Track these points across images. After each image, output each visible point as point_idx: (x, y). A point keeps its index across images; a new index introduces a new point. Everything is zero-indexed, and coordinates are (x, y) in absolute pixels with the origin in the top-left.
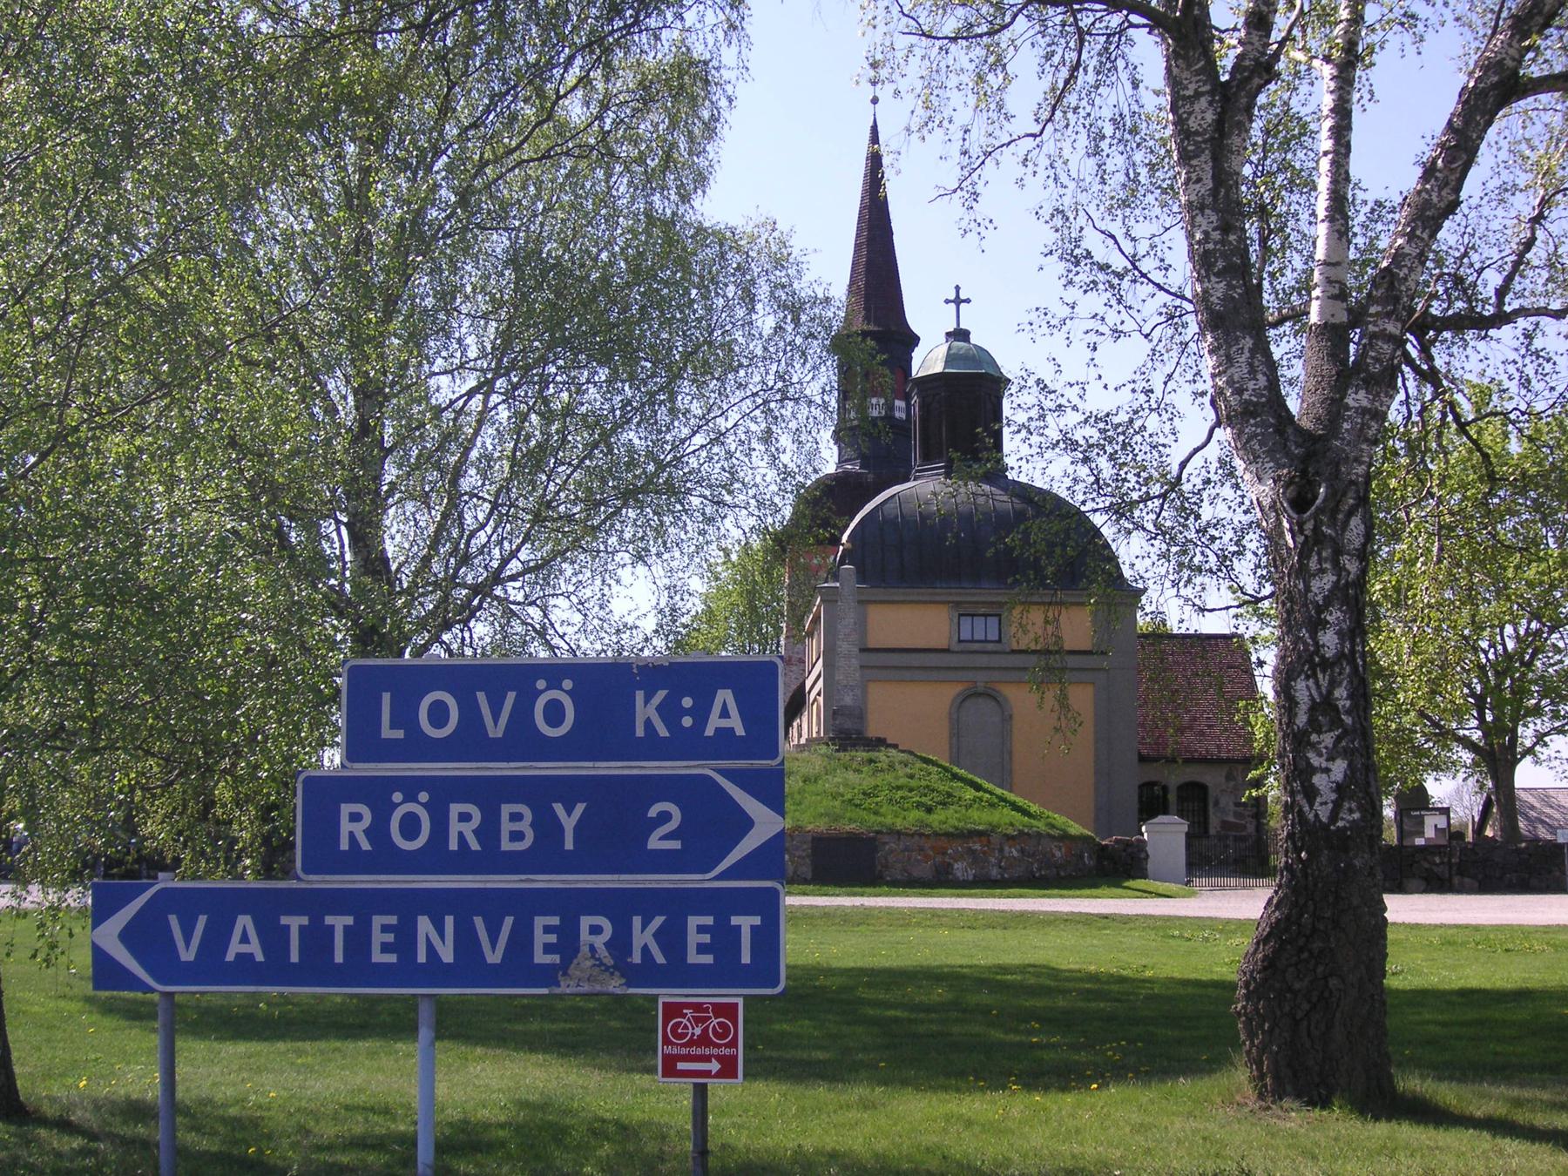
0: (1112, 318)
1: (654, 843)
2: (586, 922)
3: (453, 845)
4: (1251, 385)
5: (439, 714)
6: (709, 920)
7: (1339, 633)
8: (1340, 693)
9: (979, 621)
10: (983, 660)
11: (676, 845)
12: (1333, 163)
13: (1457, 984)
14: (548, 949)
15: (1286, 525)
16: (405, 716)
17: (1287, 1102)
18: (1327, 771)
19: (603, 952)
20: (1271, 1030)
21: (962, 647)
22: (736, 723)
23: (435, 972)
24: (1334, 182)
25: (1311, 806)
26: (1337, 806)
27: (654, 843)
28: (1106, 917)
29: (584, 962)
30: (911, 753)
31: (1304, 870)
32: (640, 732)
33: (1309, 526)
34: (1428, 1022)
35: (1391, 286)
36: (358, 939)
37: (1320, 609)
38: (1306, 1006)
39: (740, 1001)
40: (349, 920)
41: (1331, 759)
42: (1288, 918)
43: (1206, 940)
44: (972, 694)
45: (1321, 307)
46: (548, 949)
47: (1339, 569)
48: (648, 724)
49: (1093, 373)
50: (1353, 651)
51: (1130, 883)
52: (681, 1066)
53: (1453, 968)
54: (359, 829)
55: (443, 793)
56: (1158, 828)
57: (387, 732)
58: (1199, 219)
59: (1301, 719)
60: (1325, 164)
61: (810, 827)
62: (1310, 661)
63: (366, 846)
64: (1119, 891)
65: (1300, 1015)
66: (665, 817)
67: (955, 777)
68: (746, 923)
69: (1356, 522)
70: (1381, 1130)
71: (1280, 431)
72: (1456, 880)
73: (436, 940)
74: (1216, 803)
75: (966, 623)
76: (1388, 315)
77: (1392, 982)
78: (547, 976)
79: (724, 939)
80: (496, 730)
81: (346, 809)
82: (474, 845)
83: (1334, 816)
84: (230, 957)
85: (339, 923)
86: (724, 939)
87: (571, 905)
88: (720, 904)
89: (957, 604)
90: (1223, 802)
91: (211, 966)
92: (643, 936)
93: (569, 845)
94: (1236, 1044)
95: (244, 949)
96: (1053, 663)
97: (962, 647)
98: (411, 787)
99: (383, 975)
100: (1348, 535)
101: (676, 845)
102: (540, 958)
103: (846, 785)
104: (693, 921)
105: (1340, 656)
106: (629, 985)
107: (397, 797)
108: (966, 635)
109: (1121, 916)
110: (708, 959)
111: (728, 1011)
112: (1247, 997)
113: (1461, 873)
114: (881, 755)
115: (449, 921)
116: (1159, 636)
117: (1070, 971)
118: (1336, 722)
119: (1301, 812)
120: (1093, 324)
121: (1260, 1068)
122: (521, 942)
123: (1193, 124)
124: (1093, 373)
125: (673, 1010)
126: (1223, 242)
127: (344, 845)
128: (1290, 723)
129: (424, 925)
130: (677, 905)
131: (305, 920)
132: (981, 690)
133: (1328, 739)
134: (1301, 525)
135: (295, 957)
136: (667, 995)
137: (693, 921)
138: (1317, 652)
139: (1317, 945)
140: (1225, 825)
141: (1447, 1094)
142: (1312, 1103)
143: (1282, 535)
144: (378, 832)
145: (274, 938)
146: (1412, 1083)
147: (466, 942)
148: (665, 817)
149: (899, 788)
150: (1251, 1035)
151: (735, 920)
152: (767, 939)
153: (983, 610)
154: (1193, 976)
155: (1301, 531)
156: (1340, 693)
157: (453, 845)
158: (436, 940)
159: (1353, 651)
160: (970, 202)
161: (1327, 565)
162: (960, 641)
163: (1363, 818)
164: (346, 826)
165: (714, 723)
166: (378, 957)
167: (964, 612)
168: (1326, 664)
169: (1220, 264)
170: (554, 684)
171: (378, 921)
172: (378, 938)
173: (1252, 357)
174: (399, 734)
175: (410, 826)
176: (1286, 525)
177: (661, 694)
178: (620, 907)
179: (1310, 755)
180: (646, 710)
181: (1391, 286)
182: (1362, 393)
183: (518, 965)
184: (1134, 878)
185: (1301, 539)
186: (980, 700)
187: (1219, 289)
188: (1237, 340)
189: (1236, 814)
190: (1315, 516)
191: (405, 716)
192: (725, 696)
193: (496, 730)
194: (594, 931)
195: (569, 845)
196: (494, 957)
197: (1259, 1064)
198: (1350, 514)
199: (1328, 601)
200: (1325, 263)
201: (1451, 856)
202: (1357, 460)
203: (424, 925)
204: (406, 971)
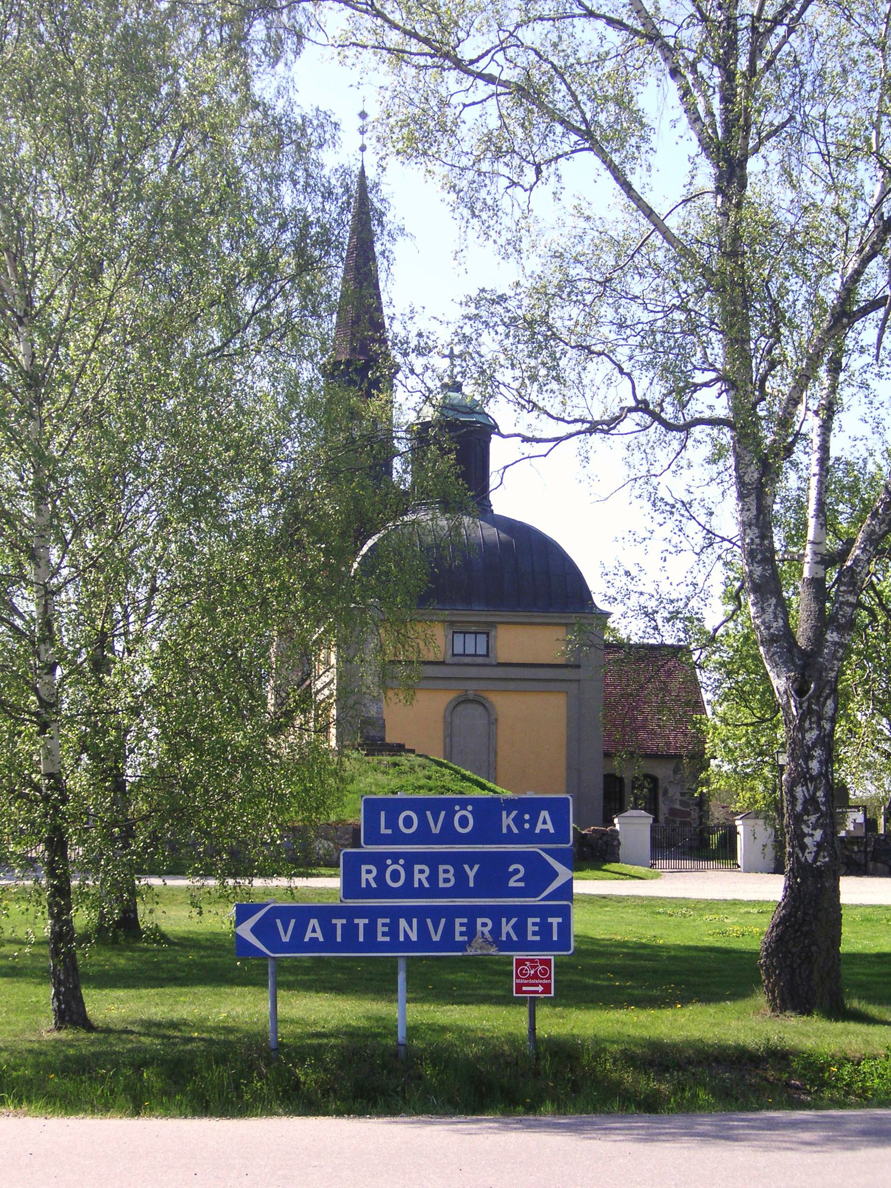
0: (675, 539)
1: (512, 883)
2: (480, 921)
3: (416, 885)
4: (775, 625)
5: (408, 822)
6: (538, 920)
7: (820, 762)
8: (820, 794)
9: (470, 638)
10: (473, 672)
11: (522, 884)
12: (819, 481)
13: (877, 950)
14: (462, 934)
15: (793, 703)
16: (392, 823)
17: (788, 1013)
18: (812, 835)
19: (487, 935)
20: (780, 974)
21: (456, 660)
22: (550, 827)
23: (408, 945)
24: (819, 493)
25: (803, 853)
26: (817, 854)
27: (512, 883)
28: (604, 897)
29: (479, 940)
30: (427, 757)
31: (799, 889)
32: (505, 831)
33: (805, 705)
34: (858, 974)
35: (852, 577)
36: (371, 930)
37: (810, 749)
38: (799, 961)
39: (552, 958)
40: (366, 921)
41: (814, 829)
42: (790, 913)
43: (684, 915)
44: (464, 701)
45: (810, 568)
46: (462, 934)
47: (820, 728)
48: (508, 826)
49: (665, 575)
50: (827, 771)
51: (607, 867)
52: (524, 988)
53: (871, 939)
54: (370, 877)
55: (411, 860)
56: (625, 820)
57: (383, 831)
58: (748, 531)
59: (799, 808)
60: (814, 481)
61: (351, 821)
62: (804, 777)
63: (374, 885)
64: (600, 873)
65: (795, 966)
66: (517, 871)
67: (464, 778)
68: (555, 921)
69: (830, 703)
70: (840, 1026)
71: (790, 651)
72: (871, 865)
73: (408, 930)
74: (665, 792)
75: (459, 638)
76: (850, 592)
77: (844, 948)
78: (461, 946)
79: (545, 929)
80: (436, 830)
81: (364, 868)
82: (426, 885)
83: (815, 859)
84: (306, 939)
85: (361, 922)
86: (545, 929)
87: (472, 913)
88: (543, 912)
89: (452, 623)
90: (671, 793)
91: (297, 943)
92: (507, 928)
93: (471, 884)
94: (759, 983)
95: (314, 935)
96: (530, 676)
97: (456, 660)
98: (395, 857)
99: (383, 947)
100: (826, 709)
101: (522, 884)
102: (458, 938)
103: (377, 785)
104: (530, 920)
105: (820, 774)
106: (500, 950)
107: (389, 862)
108: (459, 649)
109: (616, 896)
110: (538, 938)
111: (547, 962)
112: (767, 956)
113: (875, 859)
114: (402, 759)
115: (415, 921)
116: (620, 646)
117: (603, 940)
118: (817, 810)
119: (797, 857)
120: (666, 545)
121: (773, 995)
122: (449, 930)
123: (747, 479)
124: (665, 575)
125: (520, 962)
126: (761, 545)
127: (364, 885)
128: (793, 809)
129: (403, 923)
130: (523, 913)
131: (344, 921)
132: (471, 697)
133: (813, 819)
134: (801, 704)
135: (339, 939)
136: (517, 955)
137: (530, 920)
138: (808, 772)
139: (805, 929)
140: (673, 812)
141: (873, 1010)
142: (802, 1013)
143: (790, 708)
144: (380, 878)
145: (328, 930)
146: (855, 1004)
147: (423, 931)
148: (517, 871)
149: (420, 788)
150: (769, 977)
151: (550, 920)
152: (565, 927)
153: (474, 629)
154: (691, 943)
155: (801, 707)
156: (820, 794)
157: (416, 885)
158: (408, 930)
159: (827, 771)
160: (584, 464)
161: (814, 726)
162: (454, 655)
163: (830, 861)
164: (364, 876)
165: (540, 827)
166: (380, 938)
167: (456, 628)
168: (812, 779)
169: (759, 557)
170: (464, 808)
171: (380, 921)
172: (380, 929)
173: (776, 609)
174: (389, 832)
175: (395, 876)
176: (793, 703)
177: (514, 813)
178: (496, 914)
179: (803, 827)
180: (507, 821)
181: (852, 577)
182: (835, 634)
183: (448, 942)
184: (610, 862)
185: (800, 711)
186: (470, 705)
187: (758, 571)
188: (767, 599)
189: (682, 803)
190: (809, 699)
191: (392, 823)
192: (544, 814)
193: (436, 830)
194: (484, 926)
195: (471, 884)
196: (436, 938)
197: (773, 992)
198: (827, 698)
199: (814, 745)
200: (813, 543)
201: (867, 845)
202: (832, 670)
203: (403, 923)
204: (394, 945)
